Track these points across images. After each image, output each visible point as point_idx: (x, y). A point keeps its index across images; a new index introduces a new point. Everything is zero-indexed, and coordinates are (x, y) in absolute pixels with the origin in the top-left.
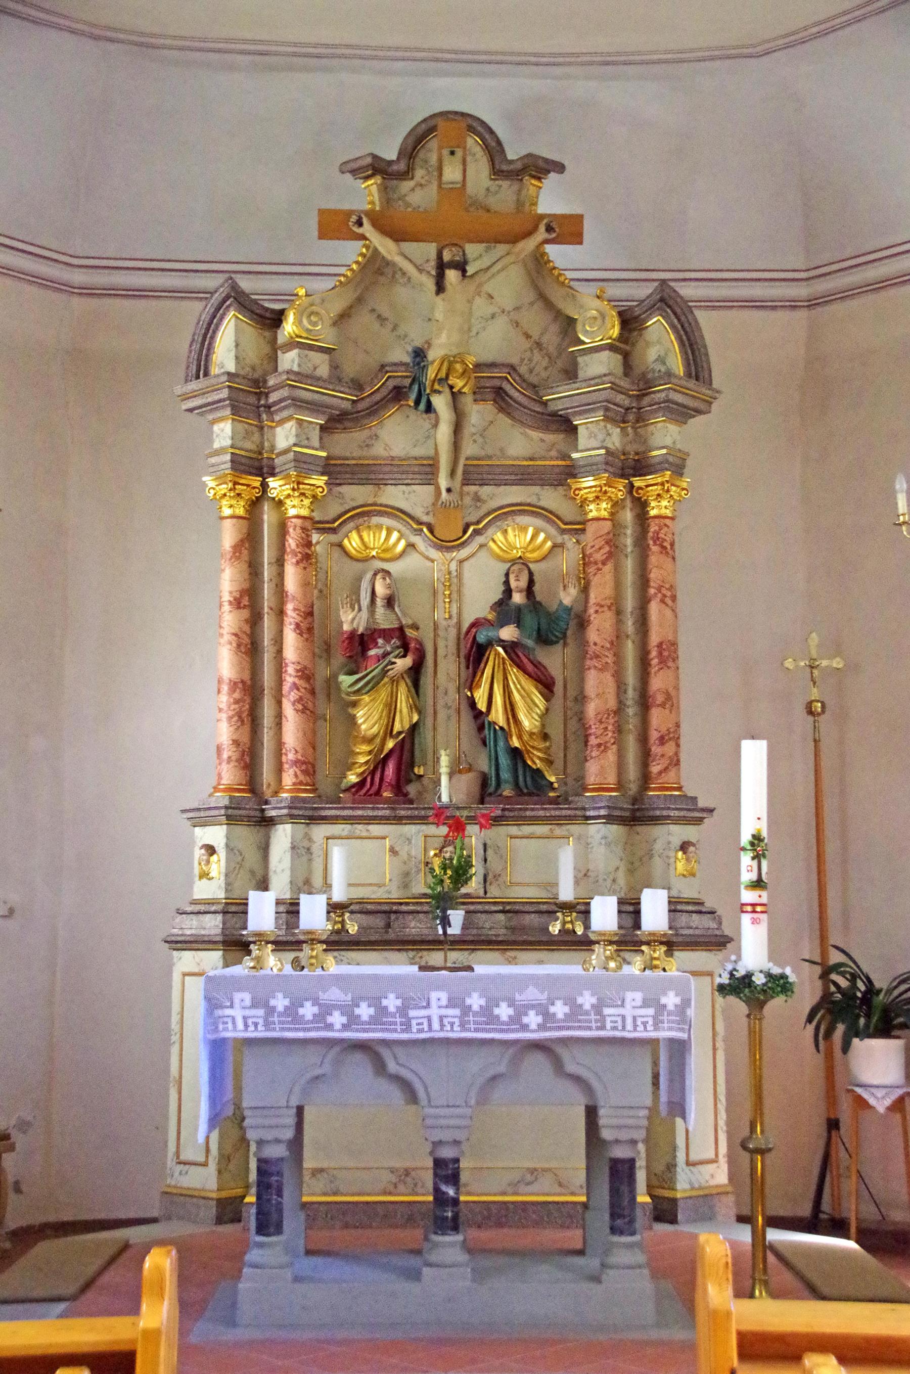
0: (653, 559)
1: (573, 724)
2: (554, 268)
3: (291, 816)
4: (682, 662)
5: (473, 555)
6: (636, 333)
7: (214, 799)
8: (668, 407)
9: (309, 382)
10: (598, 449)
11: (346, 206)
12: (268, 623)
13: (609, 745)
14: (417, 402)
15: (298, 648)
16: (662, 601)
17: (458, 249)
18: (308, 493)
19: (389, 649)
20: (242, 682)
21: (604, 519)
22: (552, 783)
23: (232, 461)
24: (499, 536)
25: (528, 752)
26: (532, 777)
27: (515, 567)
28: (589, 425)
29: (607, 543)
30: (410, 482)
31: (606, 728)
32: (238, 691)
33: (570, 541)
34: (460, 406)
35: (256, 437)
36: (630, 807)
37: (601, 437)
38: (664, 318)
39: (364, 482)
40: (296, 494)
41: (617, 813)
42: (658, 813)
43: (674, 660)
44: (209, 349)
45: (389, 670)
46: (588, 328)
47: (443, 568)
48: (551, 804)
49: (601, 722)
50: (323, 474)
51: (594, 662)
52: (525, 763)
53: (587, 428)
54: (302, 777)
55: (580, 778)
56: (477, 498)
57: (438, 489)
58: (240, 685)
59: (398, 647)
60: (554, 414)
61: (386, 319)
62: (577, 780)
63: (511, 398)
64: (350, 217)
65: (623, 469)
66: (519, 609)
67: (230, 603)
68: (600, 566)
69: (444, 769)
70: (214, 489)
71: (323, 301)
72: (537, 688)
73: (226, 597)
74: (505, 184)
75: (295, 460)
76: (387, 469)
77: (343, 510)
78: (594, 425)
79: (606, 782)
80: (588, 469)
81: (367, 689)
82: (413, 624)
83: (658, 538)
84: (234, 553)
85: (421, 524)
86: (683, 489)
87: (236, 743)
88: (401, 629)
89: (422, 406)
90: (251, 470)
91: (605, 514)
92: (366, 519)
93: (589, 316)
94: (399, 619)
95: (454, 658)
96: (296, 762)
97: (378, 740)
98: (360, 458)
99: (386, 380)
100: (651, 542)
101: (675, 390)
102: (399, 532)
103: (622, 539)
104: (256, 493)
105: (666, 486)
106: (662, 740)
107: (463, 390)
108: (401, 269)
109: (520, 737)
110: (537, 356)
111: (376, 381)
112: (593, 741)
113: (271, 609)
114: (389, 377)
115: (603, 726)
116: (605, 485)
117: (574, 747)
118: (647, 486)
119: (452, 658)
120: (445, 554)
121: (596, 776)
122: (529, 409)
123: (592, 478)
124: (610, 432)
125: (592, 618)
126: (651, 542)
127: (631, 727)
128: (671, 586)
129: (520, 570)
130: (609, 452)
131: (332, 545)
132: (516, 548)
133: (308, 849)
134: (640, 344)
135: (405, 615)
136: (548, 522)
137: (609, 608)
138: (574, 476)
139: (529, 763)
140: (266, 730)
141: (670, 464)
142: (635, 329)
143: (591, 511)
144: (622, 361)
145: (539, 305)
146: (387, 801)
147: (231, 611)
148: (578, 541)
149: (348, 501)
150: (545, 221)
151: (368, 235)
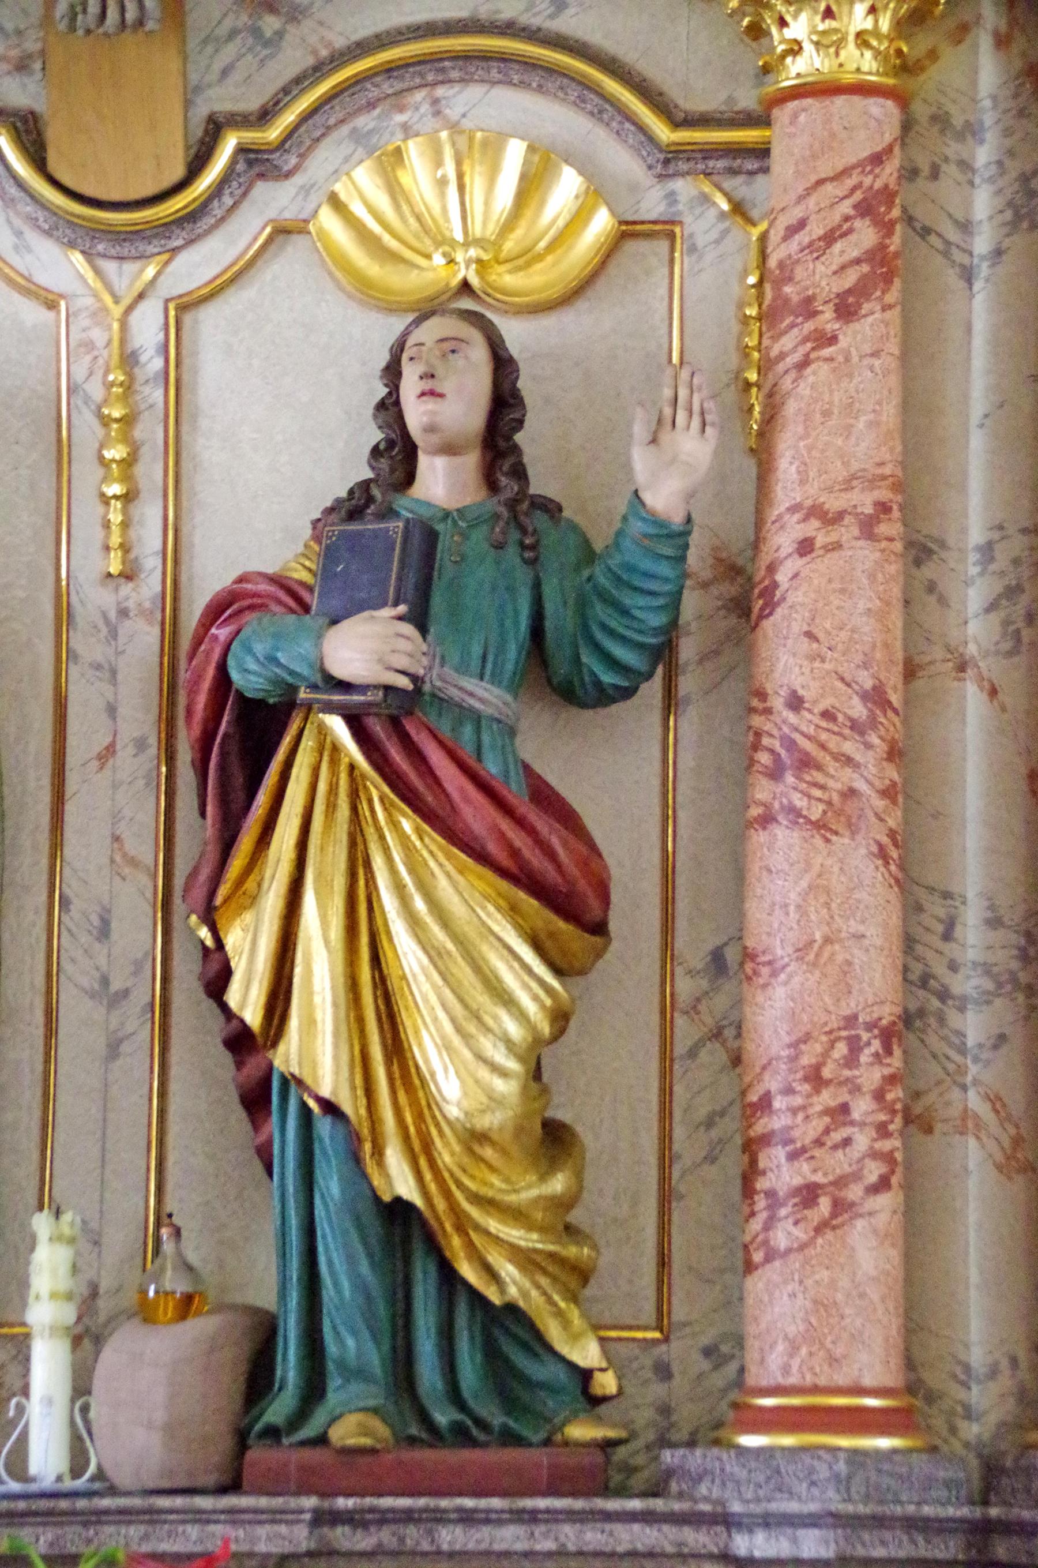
13: (854, 1192)
22: (586, 1375)
26: (492, 1354)
29: (864, 209)
31: (844, 1109)
36: (964, 1512)
47: (98, 336)
48: (552, 1491)
49: (816, 1079)
52: (448, 1274)
68: (827, 319)
72: (513, 911)
79: (841, 1379)
103: (947, 187)
115: (827, 1098)
120: (110, 267)
121: (794, 1349)
125: (782, 577)
127: (974, 1100)
129: (451, 346)
132: (442, 241)
136: (597, 115)
137: (868, 528)
139: (468, 1271)
143: (795, 49)
148: (739, 209)
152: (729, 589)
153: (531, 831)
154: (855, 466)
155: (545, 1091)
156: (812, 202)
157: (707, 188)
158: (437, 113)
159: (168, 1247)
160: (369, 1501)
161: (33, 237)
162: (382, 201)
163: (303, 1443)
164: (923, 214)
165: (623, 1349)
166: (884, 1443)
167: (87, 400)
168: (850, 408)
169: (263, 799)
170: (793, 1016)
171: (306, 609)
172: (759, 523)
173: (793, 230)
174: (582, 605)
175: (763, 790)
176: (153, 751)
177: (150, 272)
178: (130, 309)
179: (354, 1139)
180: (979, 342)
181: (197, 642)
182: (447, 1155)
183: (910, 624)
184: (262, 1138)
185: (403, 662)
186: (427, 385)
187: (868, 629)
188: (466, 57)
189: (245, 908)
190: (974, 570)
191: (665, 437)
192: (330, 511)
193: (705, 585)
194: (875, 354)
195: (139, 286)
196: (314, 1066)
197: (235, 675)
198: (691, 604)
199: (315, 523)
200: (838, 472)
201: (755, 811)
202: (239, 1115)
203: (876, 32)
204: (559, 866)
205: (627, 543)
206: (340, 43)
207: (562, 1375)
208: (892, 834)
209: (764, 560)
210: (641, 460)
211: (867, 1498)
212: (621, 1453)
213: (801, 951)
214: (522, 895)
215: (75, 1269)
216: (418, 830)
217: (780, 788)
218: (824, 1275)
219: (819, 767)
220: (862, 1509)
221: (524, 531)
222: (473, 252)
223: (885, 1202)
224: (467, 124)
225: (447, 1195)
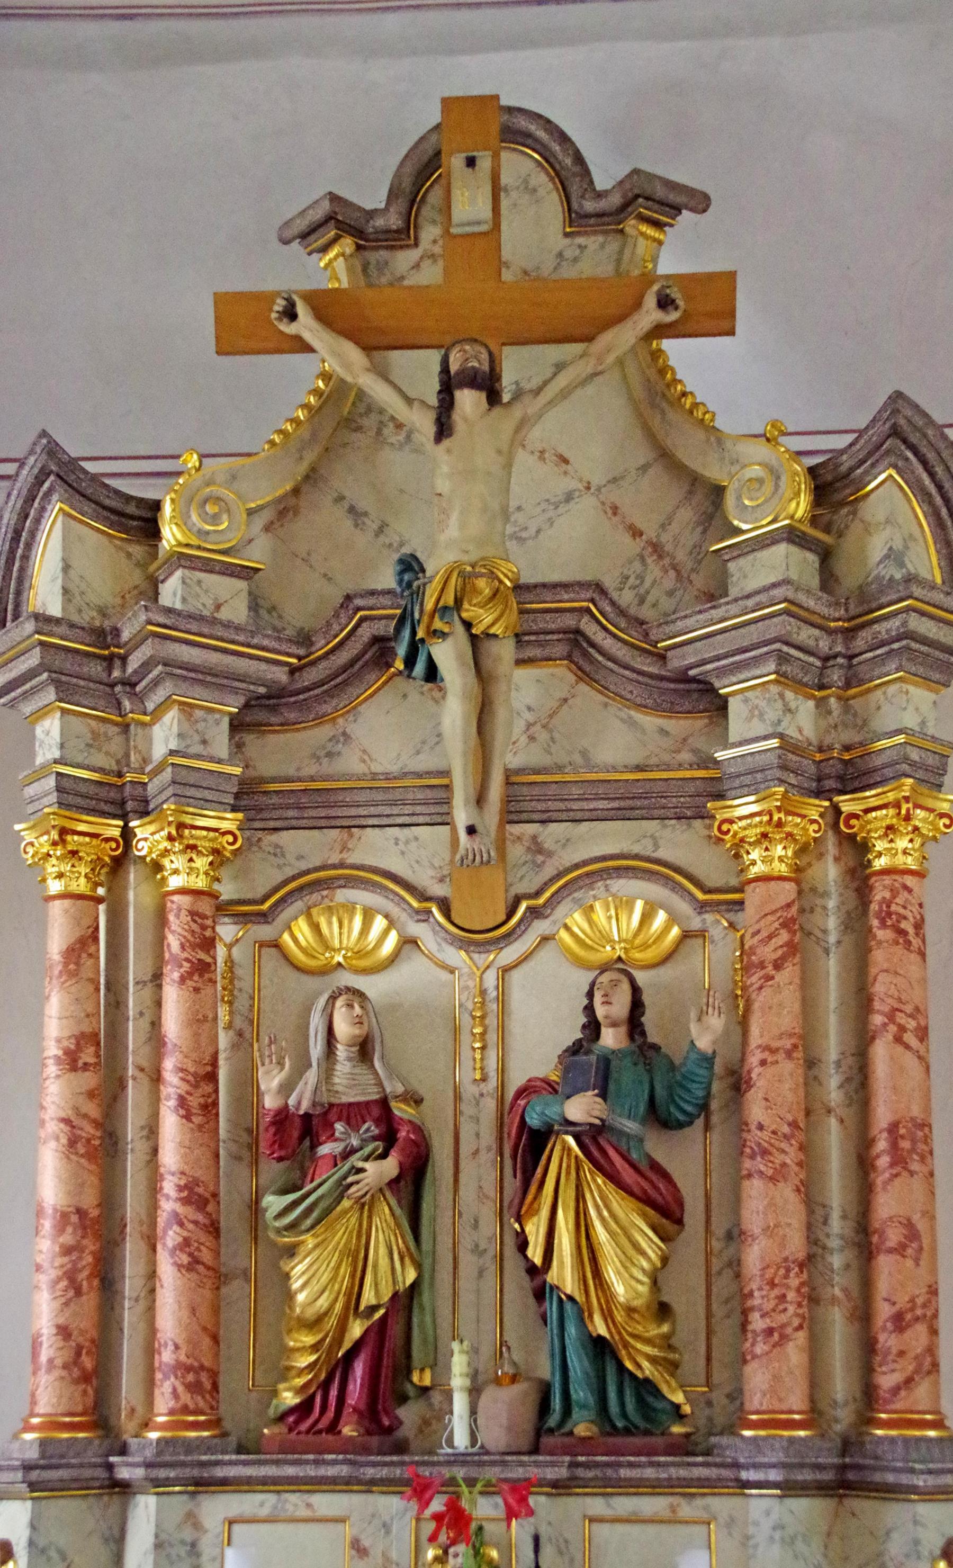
0: (879, 957)
1: (723, 1285)
2: (684, 394)
3: (157, 1483)
4: (939, 1163)
5: (525, 958)
6: (844, 511)
7: (16, 1445)
8: (908, 648)
9: (194, 627)
10: (766, 738)
11: (270, 286)
12: (134, 1094)
13: (789, 1330)
14: (410, 662)
15: (181, 1145)
16: (898, 1039)
17: (479, 348)
18: (203, 845)
19: (355, 1142)
20: (80, 1212)
21: (781, 878)
22: (677, 1407)
23: (59, 789)
24: (577, 919)
25: (626, 1345)
27: (605, 978)
28: (749, 694)
29: (784, 925)
30: (407, 820)
31: (784, 1296)
32: (69, 1230)
33: (716, 924)
34: (487, 663)
35: (116, 745)
36: (836, 1460)
37: (772, 714)
38: (899, 473)
39: (323, 823)
40: (177, 846)
41: (806, 1476)
42: (890, 1478)
43: (923, 1159)
44: (20, 581)
45: (351, 1184)
46: (747, 502)
47: (471, 984)
49: (772, 1284)
50: (234, 809)
51: (759, 1164)
52: (621, 1368)
53: (746, 701)
54: (186, 1398)
55: (736, 1395)
56: (536, 847)
57: (454, 831)
58: (74, 1218)
59: (375, 1138)
60: (683, 677)
61: (366, 514)
62: (731, 1397)
63: (593, 645)
64: (274, 303)
65: (819, 780)
66: (606, 1062)
67: (58, 1059)
68: (770, 970)
69: (458, 1381)
70: (32, 844)
71: (234, 478)
72: (644, 1216)
73: (53, 1050)
74: (592, 242)
75: (174, 782)
76: (362, 797)
77: (280, 878)
78: (757, 692)
79: (784, 1407)
80: (747, 780)
81: (309, 1222)
82: (406, 1092)
83: (889, 914)
84: (66, 964)
85: (429, 899)
86: (942, 816)
87: (64, 1332)
88: (384, 1103)
89: (420, 668)
90: (106, 808)
91: (782, 869)
92: (325, 893)
93: (748, 476)
94: (380, 1084)
95: (492, 1155)
96: (181, 1368)
97: (332, 1322)
98: (313, 779)
99: (358, 625)
100: (875, 923)
101: (923, 614)
102: (386, 916)
103: (817, 918)
104: (109, 851)
105: (904, 807)
106: (899, 1322)
107: (492, 631)
108: (393, 418)
109: (608, 1316)
110: (654, 570)
111: (336, 627)
112: (757, 1323)
113: (142, 1070)
114: (363, 620)
115: (777, 1292)
116: (779, 809)
117: (725, 1330)
118: (867, 811)
119: (488, 1157)
120: (476, 956)
122: (633, 670)
123: (752, 798)
124: (793, 705)
125: (754, 1075)
126: (875, 923)
127: (837, 1291)
128: (917, 1009)
129: (615, 984)
130: (787, 745)
131: (262, 945)
132: (611, 941)
133: (193, 1545)
134: (856, 528)
135: (392, 1072)
136: (673, 890)
137: (789, 1054)
138: (720, 796)
139: (629, 1365)
140: (127, 1304)
141: (913, 764)
142: (843, 504)
143: (754, 863)
144: (817, 565)
145: (657, 472)
146: (347, 1447)
147: (58, 1076)
148: (732, 925)
149: (293, 861)
150: (656, 288)
151: (307, 336)
152: (731, 1080)
153: (651, 1182)
154: (783, 1029)
155: (659, 1290)
156: (762, 923)
157: (718, 917)
158: (607, 890)
159: (506, 1355)
160: (591, 1458)
161: (444, 945)
162: (586, 926)
163: (563, 1434)
164: (808, 927)
165: (693, 1396)
166: (802, 1433)
167: (466, 1009)
168: (781, 1005)
169: (539, 1171)
170: (762, 1258)
171: (556, 1091)
172: (744, 1054)
173: (754, 934)
174: (670, 1088)
175: (747, 1164)
176: (494, 1151)
177: (492, 957)
178: (483, 972)
179: (580, 1312)
180: (833, 979)
181: (511, 1108)
182: (619, 1317)
183: (807, 1095)
184: (542, 1309)
185: (597, 1113)
186: (604, 999)
187: (790, 1097)
188: (617, 869)
189: (533, 1215)
190: (833, 1071)
191: (705, 1018)
192: (565, 1051)
193: (721, 1078)
194: (790, 984)
195: (487, 963)
196: (564, 1280)
197: (527, 1120)
198: (716, 1087)
199: (559, 1057)
200: (776, 1031)
201: (745, 1172)
202: (531, 1301)
203: (786, 856)
204: (661, 1194)
205: (689, 1063)
206: (568, 864)
207: (669, 1407)
208: (801, 1181)
209: (746, 1068)
210: (694, 1028)
211: (795, 1457)
212: (693, 1437)
213: (766, 1229)
214: (648, 1209)
215: (469, 1364)
216: (604, 1183)
217: (755, 1163)
218: (777, 1365)
219: (770, 1154)
220: (793, 1460)
221: (645, 1057)
222: (622, 945)
223: (801, 1336)
224: (619, 894)
225: (619, 1333)
